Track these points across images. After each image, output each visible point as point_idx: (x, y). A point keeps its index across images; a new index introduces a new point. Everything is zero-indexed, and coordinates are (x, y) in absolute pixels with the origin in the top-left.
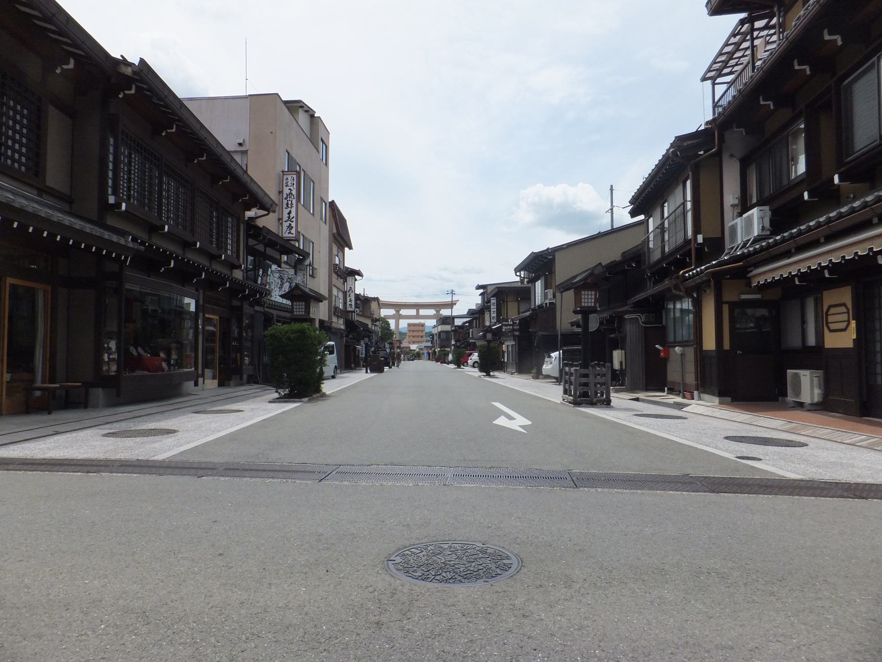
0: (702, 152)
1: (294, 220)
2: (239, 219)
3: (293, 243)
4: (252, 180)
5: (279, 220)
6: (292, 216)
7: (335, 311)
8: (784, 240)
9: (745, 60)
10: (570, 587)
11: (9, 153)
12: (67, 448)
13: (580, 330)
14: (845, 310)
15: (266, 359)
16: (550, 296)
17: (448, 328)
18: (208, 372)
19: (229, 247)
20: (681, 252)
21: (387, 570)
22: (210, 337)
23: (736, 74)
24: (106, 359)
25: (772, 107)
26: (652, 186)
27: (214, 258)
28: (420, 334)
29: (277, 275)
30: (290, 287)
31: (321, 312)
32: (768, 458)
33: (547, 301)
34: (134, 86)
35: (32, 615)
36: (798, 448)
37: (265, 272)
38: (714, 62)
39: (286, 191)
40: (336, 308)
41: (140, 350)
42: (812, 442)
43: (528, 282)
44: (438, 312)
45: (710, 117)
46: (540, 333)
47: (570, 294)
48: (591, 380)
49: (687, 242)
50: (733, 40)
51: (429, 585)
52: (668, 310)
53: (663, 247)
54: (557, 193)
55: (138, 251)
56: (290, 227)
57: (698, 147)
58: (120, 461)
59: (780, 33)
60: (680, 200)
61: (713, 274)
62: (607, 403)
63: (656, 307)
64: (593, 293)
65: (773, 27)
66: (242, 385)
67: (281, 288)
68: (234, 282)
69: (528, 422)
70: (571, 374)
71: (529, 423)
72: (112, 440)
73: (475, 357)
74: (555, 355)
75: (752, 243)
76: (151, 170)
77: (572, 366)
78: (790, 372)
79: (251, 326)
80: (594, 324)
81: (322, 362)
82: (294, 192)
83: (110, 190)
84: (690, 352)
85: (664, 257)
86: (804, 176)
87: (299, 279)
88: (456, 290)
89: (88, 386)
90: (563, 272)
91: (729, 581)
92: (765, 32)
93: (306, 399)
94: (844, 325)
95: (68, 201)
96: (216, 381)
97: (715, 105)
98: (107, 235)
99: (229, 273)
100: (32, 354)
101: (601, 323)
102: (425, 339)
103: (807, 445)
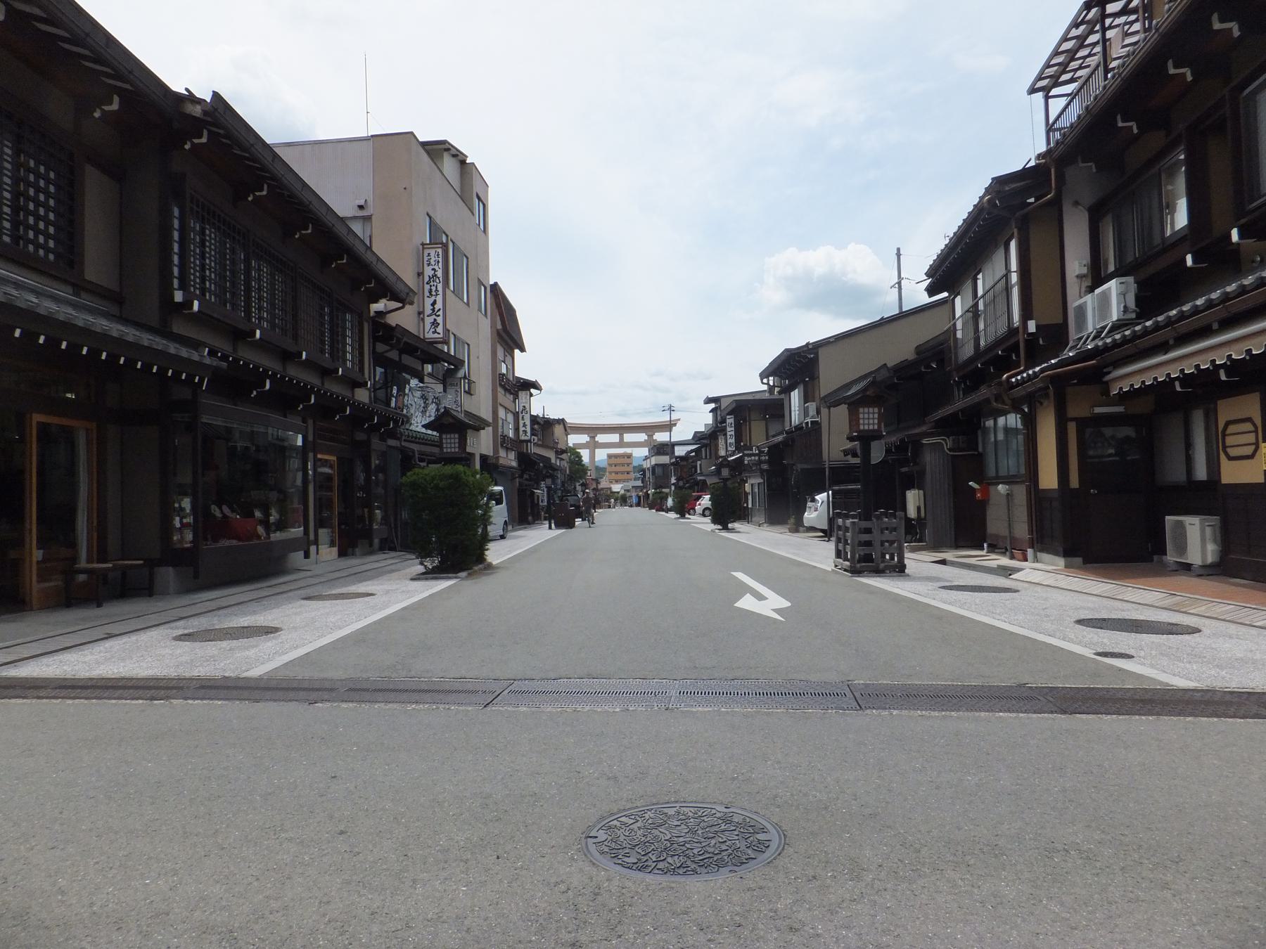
0: (1032, 200)
1: (440, 313)
2: (361, 315)
3: (439, 346)
4: (379, 259)
5: (419, 313)
6: (437, 307)
7: (503, 442)
8: (1157, 327)
9: (1092, 61)
10: (858, 878)
11: (31, 234)
12: (123, 660)
13: (857, 461)
14: (1252, 428)
15: (405, 515)
16: (812, 411)
17: (665, 459)
18: (324, 533)
19: (349, 356)
20: (1004, 346)
21: (586, 852)
22: (324, 483)
23: (1083, 80)
24: (178, 525)
25: (1135, 131)
26: (959, 249)
27: (327, 373)
28: (626, 469)
29: (418, 394)
30: (438, 410)
31: (482, 443)
32: (1142, 653)
33: (809, 420)
34: (205, 133)
35: (67, 940)
36: (1187, 637)
37: (401, 390)
38: (1047, 65)
39: (428, 272)
40: (504, 437)
41: (226, 509)
42: (1207, 626)
43: (780, 393)
44: (650, 436)
45: (1042, 148)
46: (799, 466)
47: (843, 410)
48: (876, 537)
49: (1012, 332)
50: (1075, 32)
51: (649, 878)
52: (986, 431)
53: (977, 340)
54: (818, 259)
55: (217, 368)
56: (435, 324)
57: (1026, 192)
58: (198, 679)
59: (1145, 19)
60: (1000, 271)
61: (1052, 379)
62: (900, 569)
63: (968, 426)
64: (876, 410)
65: (1135, 11)
66: (371, 553)
67: (424, 412)
68: (357, 406)
69: (785, 604)
70: (847, 529)
71: (786, 604)
72: (187, 645)
73: (706, 501)
74: (821, 497)
75: (1109, 332)
76: (233, 251)
77: (846, 516)
78: (1169, 519)
79: (382, 469)
80: (877, 453)
81: (486, 520)
82: (439, 273)
83: (176, 283)
84: (1020, 492)
85: (978, 353)
86: (1186, 232)
87: (448, 401)
88: (676, 405)
89: (152, 564)
90: (830, 377)
91: (1098, 865)
92: (1122, 19)
93: (463, 574)
94: (1248, 450)
95: (115, 301)
96: (335, 550)
97: (1050, 129)
98: (172, 348)
99: (349, 394)
100: (73, 511)
101: (888, 451)
102: (632, 475)
103: (1200, 631)
